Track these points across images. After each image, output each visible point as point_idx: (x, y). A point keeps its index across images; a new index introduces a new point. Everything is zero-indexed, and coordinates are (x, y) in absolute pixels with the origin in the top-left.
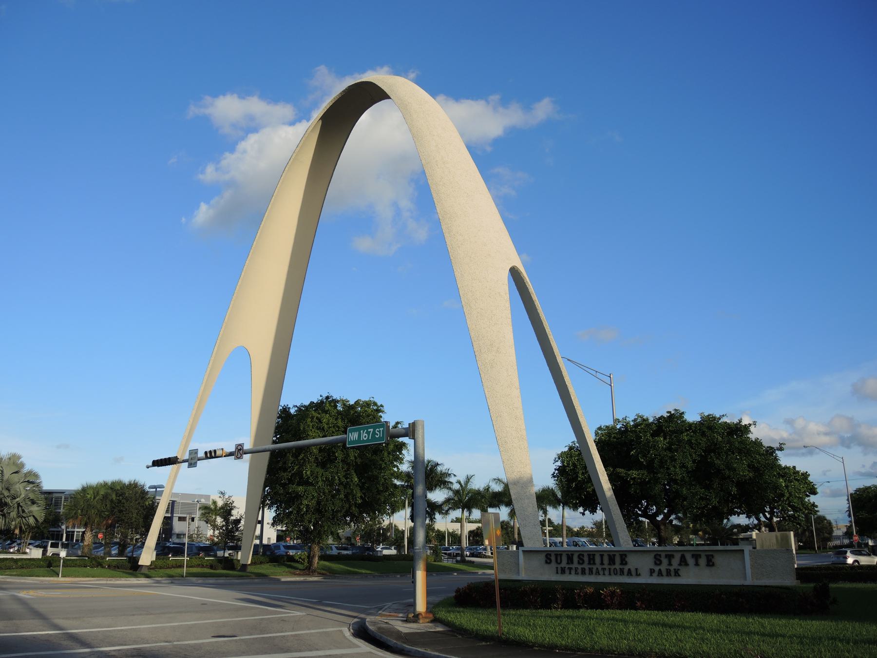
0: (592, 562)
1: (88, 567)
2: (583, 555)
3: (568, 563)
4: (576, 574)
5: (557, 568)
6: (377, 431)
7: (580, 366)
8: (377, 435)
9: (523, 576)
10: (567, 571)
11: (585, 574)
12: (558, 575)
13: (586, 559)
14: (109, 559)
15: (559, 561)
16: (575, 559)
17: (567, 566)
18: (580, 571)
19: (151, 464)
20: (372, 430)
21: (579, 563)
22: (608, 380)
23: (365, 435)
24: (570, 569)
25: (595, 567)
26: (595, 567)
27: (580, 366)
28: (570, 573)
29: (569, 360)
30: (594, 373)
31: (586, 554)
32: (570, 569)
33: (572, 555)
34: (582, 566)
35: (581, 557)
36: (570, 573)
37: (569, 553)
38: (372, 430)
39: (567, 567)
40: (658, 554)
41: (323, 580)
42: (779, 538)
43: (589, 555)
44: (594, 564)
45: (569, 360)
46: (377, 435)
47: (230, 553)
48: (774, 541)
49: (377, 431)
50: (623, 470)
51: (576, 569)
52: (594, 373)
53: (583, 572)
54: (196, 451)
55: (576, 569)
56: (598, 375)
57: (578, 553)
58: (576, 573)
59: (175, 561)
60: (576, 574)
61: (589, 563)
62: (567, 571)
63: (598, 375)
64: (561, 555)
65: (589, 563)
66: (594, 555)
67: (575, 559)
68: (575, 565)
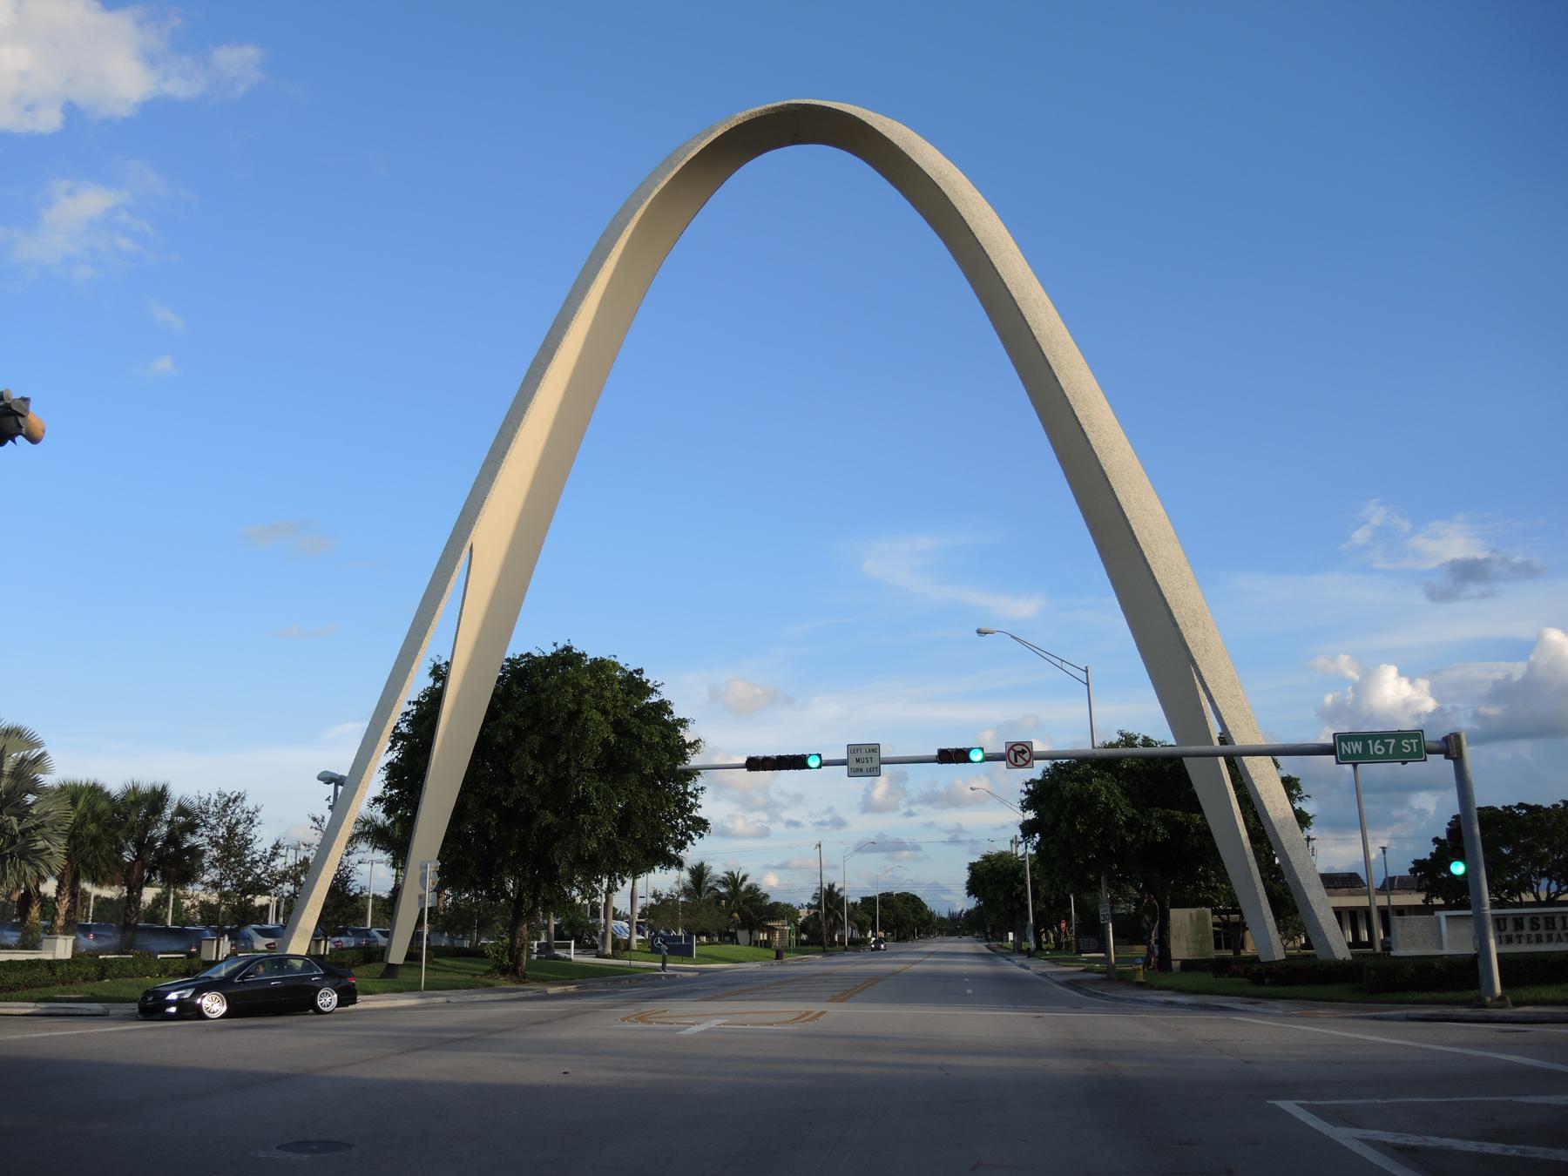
0: (1551, 926)
1: (148, 977)
2: (1538, 919)
3: (1516, 930)
4: (1528, 942)
5: (1500, 937)
6: (1405, 743)
7: (1036, 650)
8: (1407, 748)
9: (1447, 950)
10: (1515, 940)
11: (1542, 941)
12: (1502, 945)
13: (1542, 923)
14: (161, 958)
15: (1502, 928)
16: (1527, 924)
17: (1515, 934)
18: (1533, 938)
19: (743, 761)
20: (1393, 741)
21: (1532, 929)
22: (1082, 676)
23: (1377, 747)
24: (1519, 937)
25: (1555, 933)
26: (1555, 933)
27: (1036, 650)
28: (1520, 942)
29: (1012, 637)
30: (1058, 663)
31: (1540, 917)
32: (1519, 937)
33: (1522, 919)
34: (1538, 932)
35: (1535, 921)
36: (1520, 942)
37: (1518, 917)
38: (1393, 741)
39: (1515, 934)
40: (1535, 918)
41: (982, 967)
42: (1195, 917)
43: (1546, 918)
44: (1554, 928)
45: (1012, 637)
46: (1407, 748)
47: (270, 944)
48: (1188, 920)
49: (1405, 743)
50: (1180, 813)
51: (1529, 936)
52: (1058, 663)
53: (1539, 940)
54: (874, 747)
55: (1529, 936)
56: (1066, 666)
57: (1560, 916)
58: (1529, 942)
59: (170, 960)
60: (1528, 942)
61: (1547, 928)
62: (1515, 940)
63: (1066, 666)
64: (1505, 920)
65: (1547, 928)
66: (1553, 918)
67: (1527, 924)
68: (1526, 931)
